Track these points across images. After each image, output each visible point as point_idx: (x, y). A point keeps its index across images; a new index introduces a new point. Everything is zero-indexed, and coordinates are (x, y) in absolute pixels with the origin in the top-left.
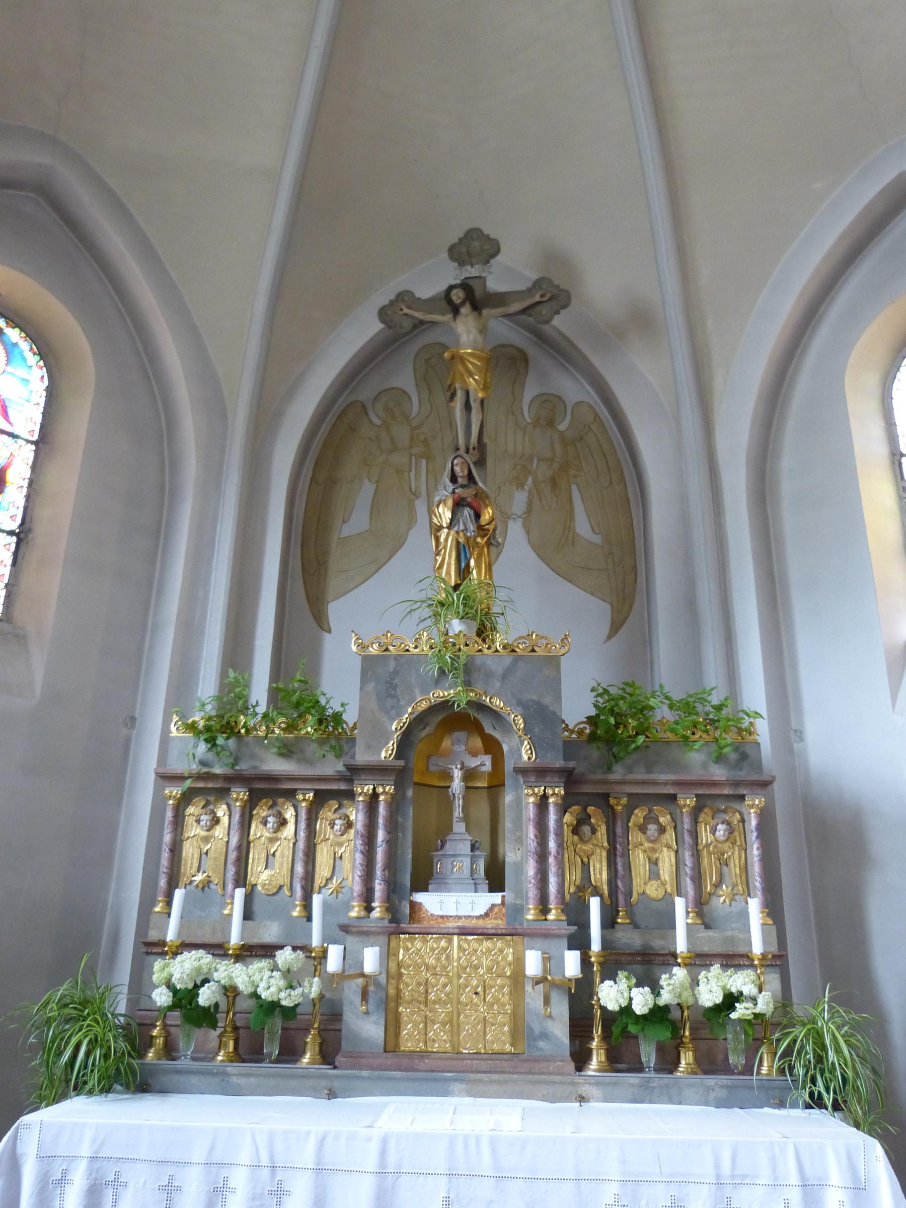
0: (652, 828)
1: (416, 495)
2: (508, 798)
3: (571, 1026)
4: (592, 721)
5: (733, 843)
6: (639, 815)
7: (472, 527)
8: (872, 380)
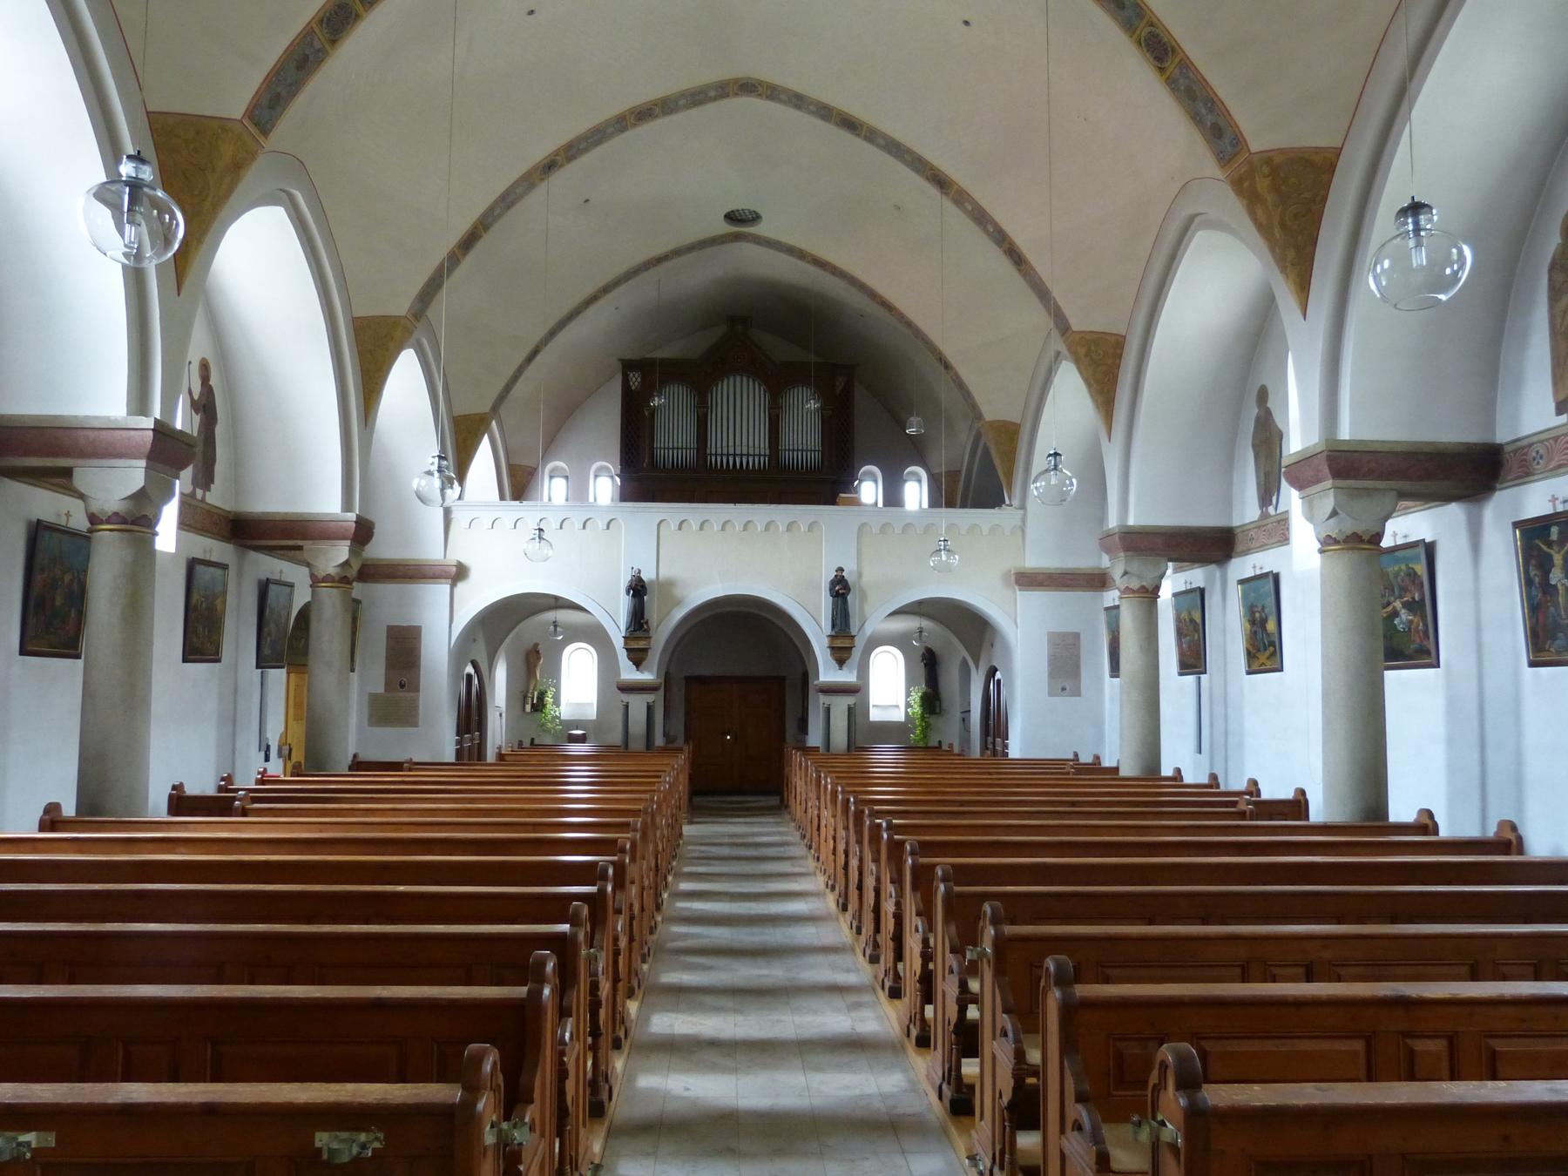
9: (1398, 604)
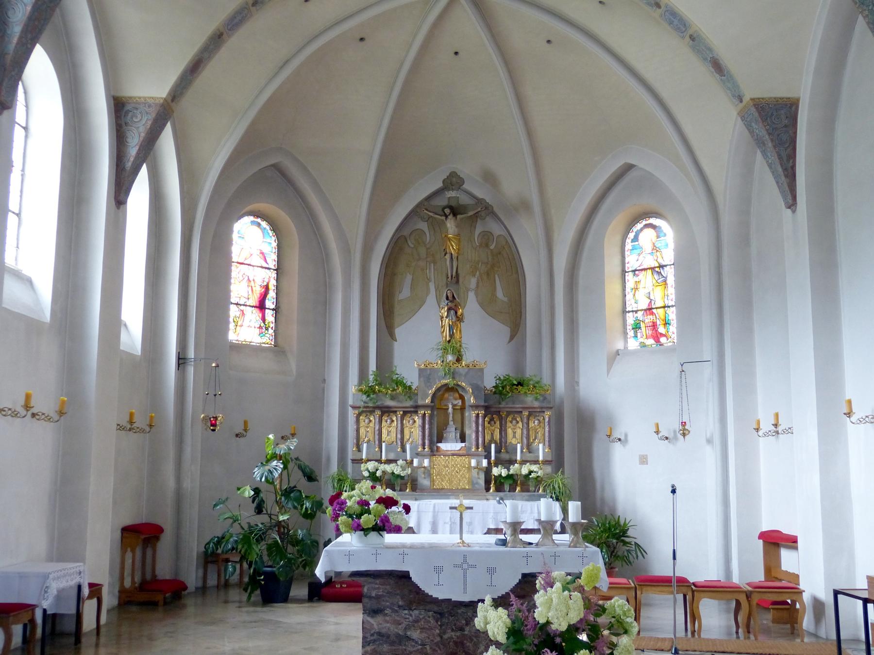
0: (514, 422)
1: (429, 280)
2: (467, 414)
4: (496, 387)
5: (541, 428)
6: (509, 419)
7: (454, 318)
8: (618, 238)
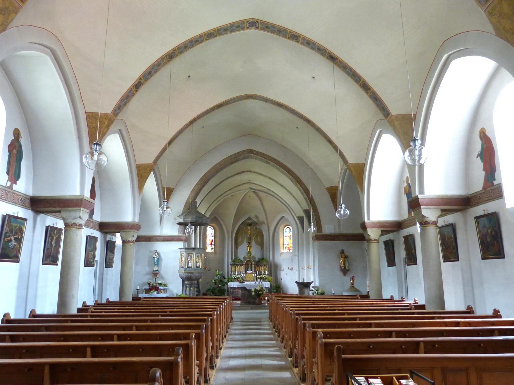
3: (422, 249)
9: (12, 238)
